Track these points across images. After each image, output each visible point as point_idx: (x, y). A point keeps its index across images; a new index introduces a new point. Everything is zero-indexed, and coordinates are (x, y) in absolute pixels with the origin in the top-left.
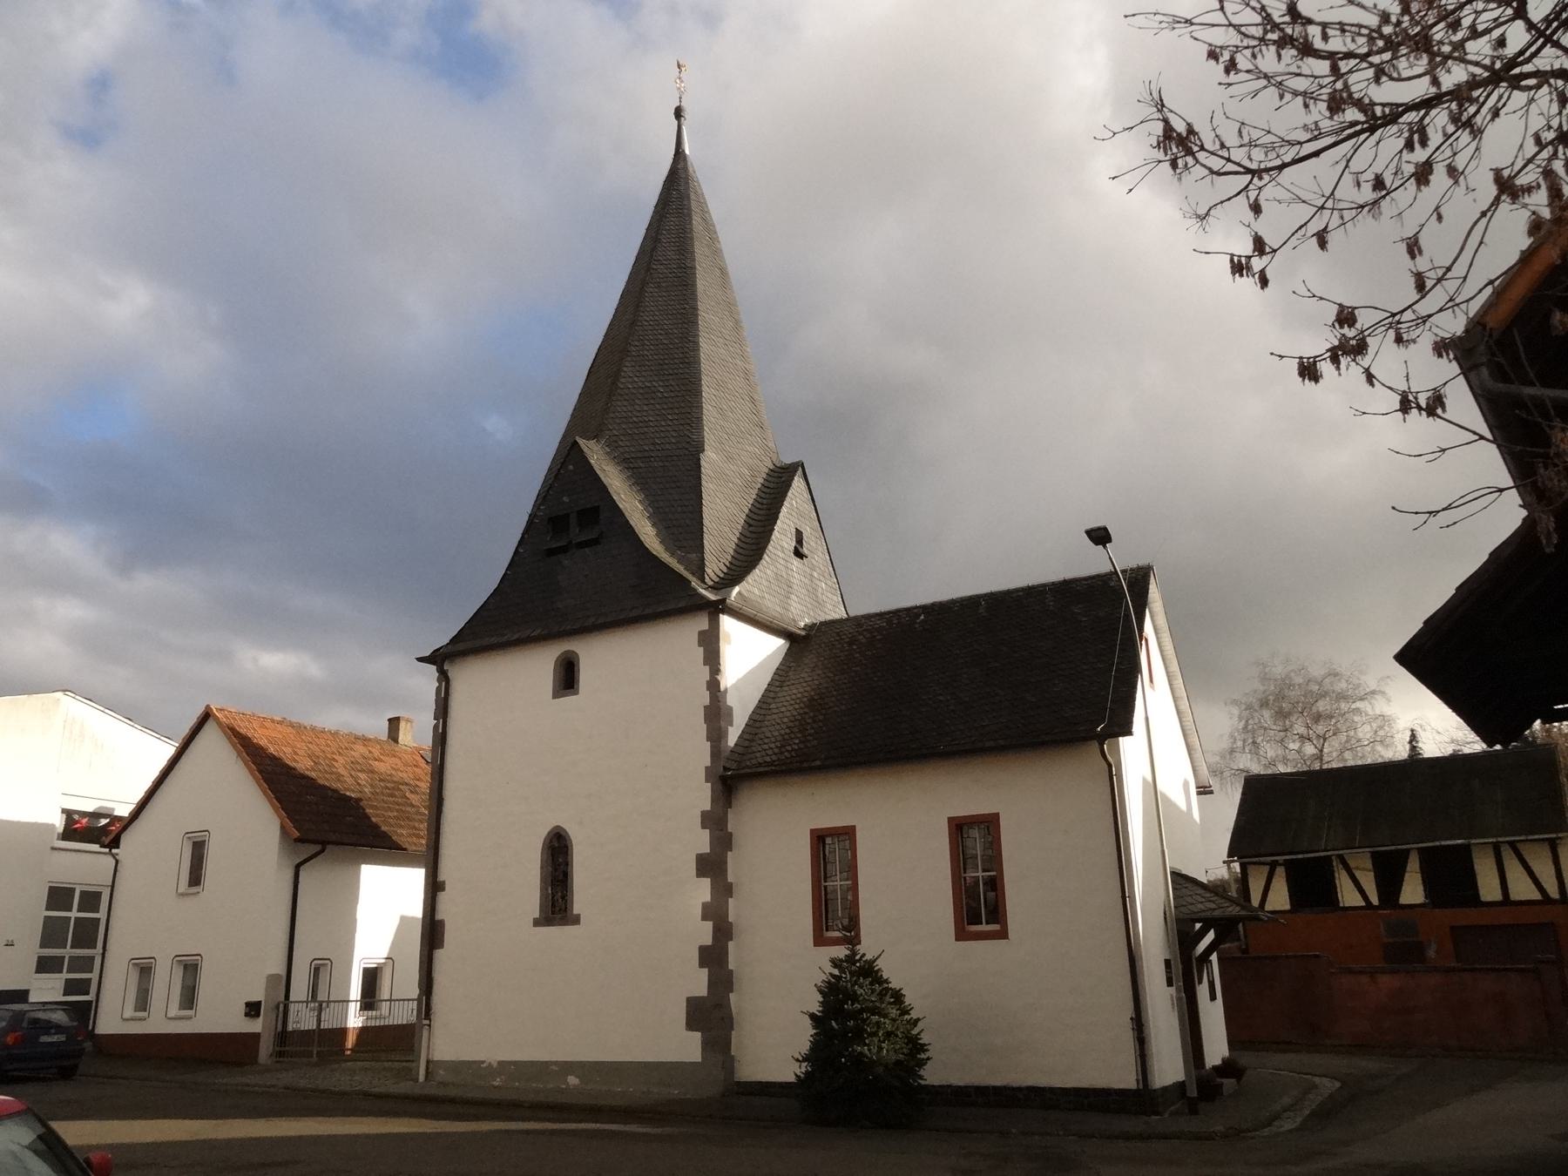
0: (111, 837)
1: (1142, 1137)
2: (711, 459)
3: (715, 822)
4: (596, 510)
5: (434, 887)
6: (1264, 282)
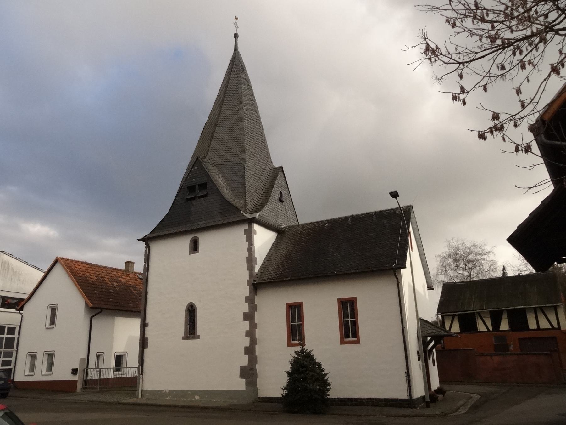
0: (20, 307)
1: (409, 416)
3: (250, 300)
5: (144, 325)
6: (464, 103)
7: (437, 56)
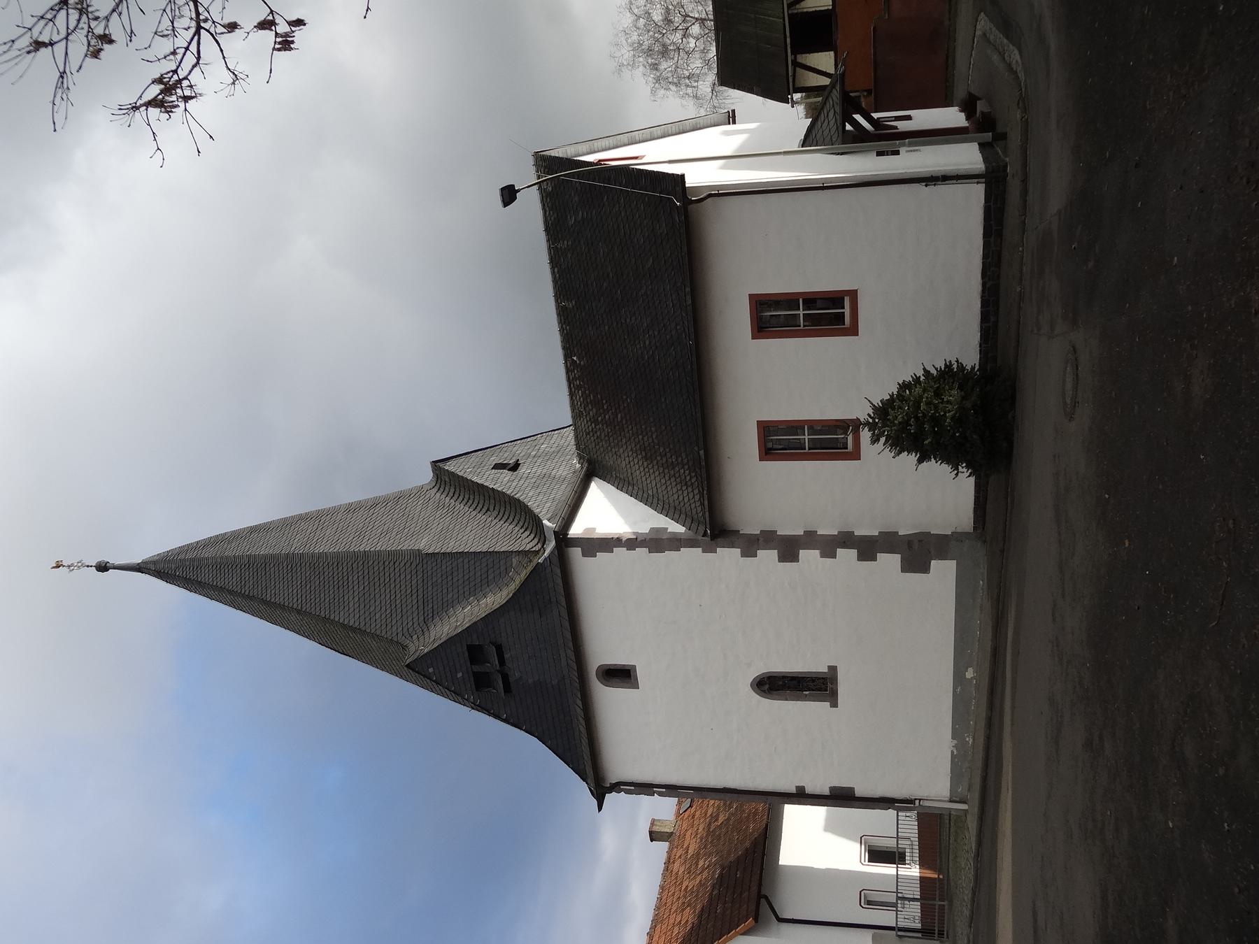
1: (1025, 181)
2: (426, 543)
3: (750, 545)
4: (471, 648)
5: (801, 796)
7: (180, 81)
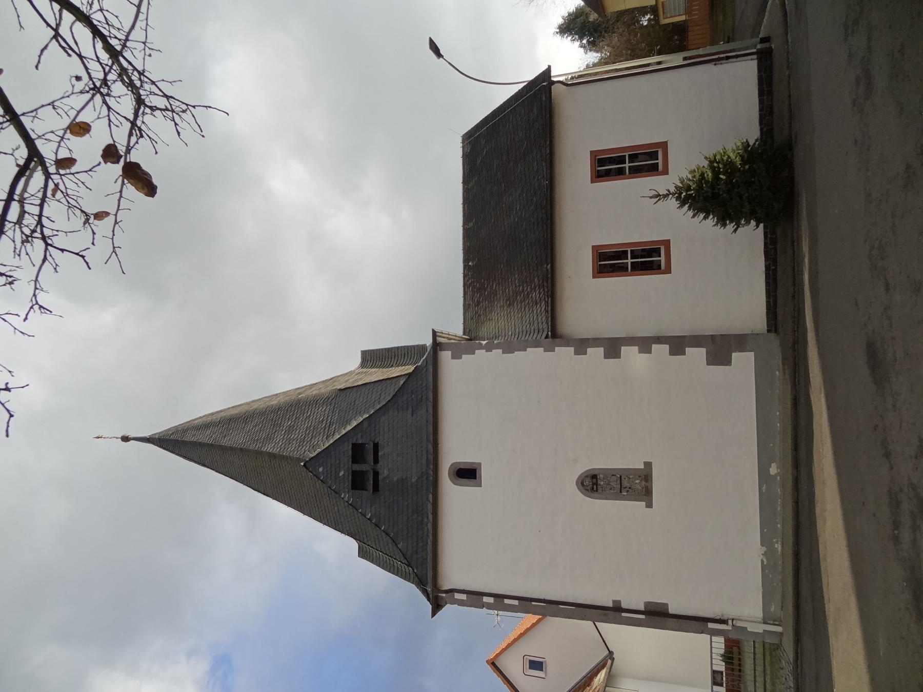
3: (582, 345)
